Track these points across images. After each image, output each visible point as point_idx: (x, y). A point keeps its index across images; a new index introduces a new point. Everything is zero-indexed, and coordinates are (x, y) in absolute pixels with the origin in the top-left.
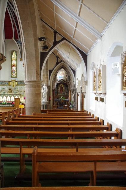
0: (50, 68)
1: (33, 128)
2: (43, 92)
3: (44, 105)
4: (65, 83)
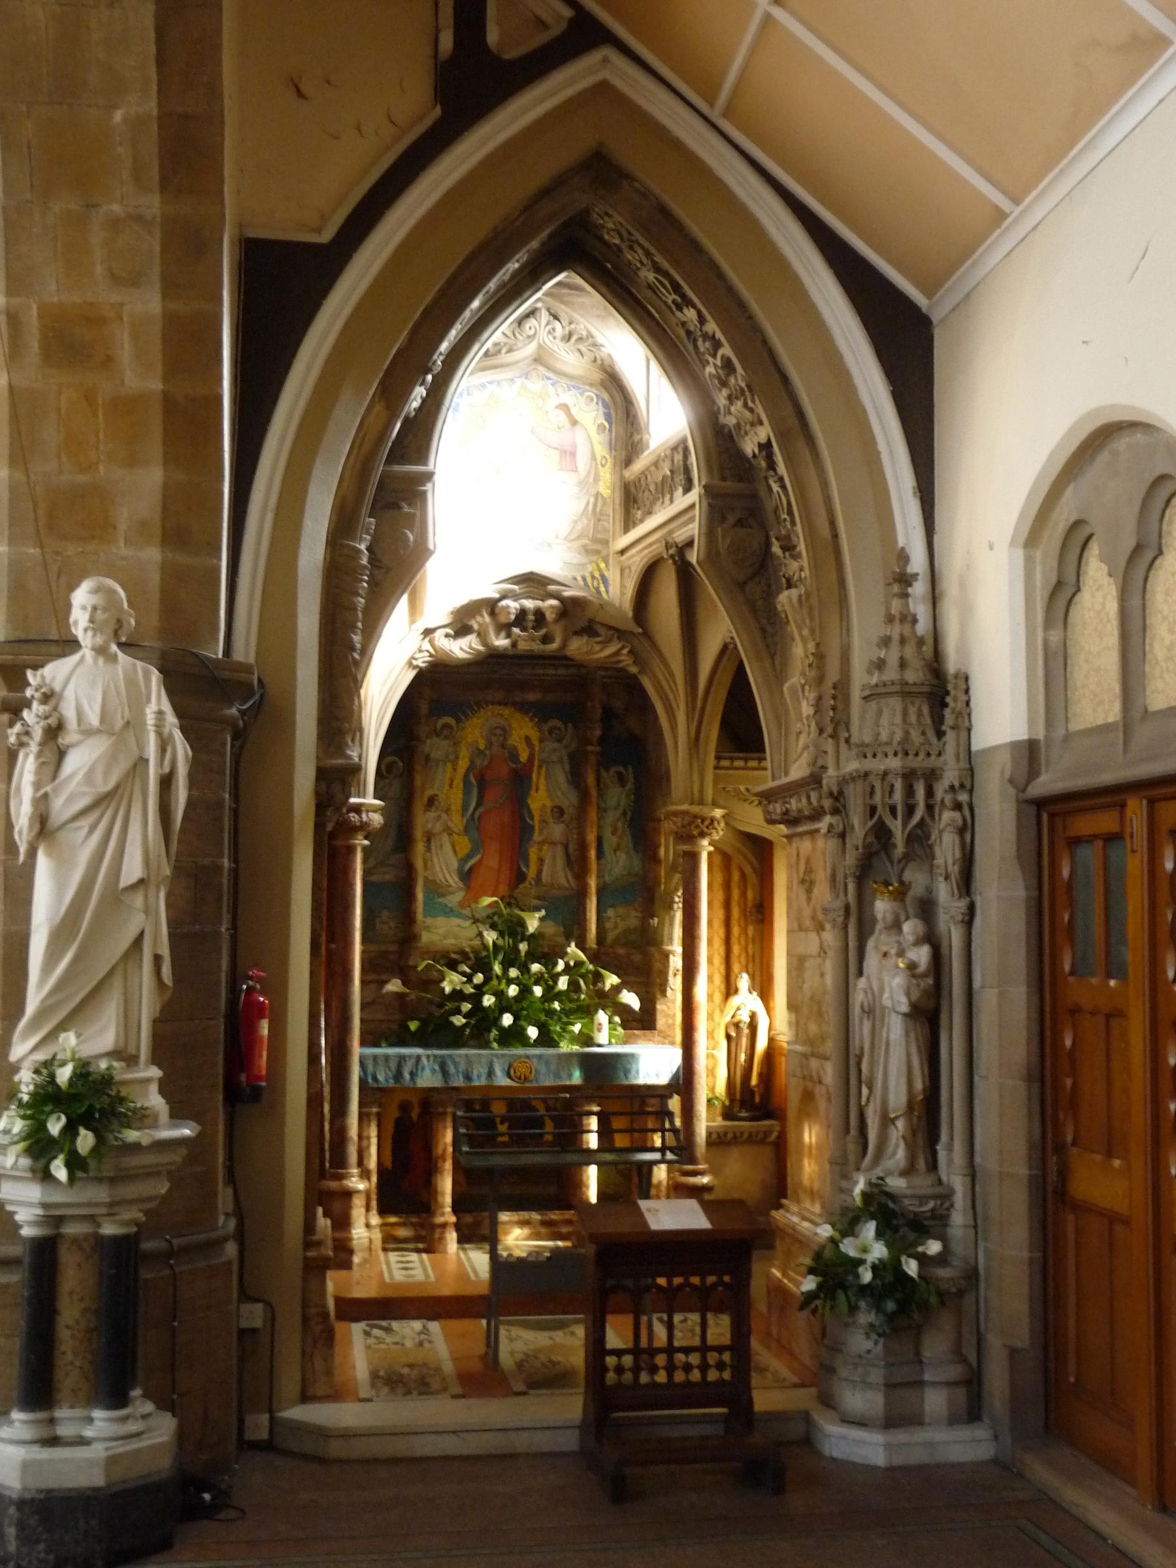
0: (280, 184)
1: (364, 1110)
2: (43, 827)
3: (45, 1252)
4: (603, 652)
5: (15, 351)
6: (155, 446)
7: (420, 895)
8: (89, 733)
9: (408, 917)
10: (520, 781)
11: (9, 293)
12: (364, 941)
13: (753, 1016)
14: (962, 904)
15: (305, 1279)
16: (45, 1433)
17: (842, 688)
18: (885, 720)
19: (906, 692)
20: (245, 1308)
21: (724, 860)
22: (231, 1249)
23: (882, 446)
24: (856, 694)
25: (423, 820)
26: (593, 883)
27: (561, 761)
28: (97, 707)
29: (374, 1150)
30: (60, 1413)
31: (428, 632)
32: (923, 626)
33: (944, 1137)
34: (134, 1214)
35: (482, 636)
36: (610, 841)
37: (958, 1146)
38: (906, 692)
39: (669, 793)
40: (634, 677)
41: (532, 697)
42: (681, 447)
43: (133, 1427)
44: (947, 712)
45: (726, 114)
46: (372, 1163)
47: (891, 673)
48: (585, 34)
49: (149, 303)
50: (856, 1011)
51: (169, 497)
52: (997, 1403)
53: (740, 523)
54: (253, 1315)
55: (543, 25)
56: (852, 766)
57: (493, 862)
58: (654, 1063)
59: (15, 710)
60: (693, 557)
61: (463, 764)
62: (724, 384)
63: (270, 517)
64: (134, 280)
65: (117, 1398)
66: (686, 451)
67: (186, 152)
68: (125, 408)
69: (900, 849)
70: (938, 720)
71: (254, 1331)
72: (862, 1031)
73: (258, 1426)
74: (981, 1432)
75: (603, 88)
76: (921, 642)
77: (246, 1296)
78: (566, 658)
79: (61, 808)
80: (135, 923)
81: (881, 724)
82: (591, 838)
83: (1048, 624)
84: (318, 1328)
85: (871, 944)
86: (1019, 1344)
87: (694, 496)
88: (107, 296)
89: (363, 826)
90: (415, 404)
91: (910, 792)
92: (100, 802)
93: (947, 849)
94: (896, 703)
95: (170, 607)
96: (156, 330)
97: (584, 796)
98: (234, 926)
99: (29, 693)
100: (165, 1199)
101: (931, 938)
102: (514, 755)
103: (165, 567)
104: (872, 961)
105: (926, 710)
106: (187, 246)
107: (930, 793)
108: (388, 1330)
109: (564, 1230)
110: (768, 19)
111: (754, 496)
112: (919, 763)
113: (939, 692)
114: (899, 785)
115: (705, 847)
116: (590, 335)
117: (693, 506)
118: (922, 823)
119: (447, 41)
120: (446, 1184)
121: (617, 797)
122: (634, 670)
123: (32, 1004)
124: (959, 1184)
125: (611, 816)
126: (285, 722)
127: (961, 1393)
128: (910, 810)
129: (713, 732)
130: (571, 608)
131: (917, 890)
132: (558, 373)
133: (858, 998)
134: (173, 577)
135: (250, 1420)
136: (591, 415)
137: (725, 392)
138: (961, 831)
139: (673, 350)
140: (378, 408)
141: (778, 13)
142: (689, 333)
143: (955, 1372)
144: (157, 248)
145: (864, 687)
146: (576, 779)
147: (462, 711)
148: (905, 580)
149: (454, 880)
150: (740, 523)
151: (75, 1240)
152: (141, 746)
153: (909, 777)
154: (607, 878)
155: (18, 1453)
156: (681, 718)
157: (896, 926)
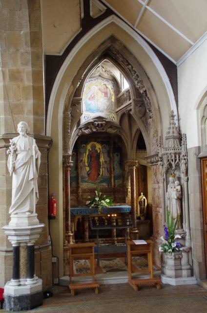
0: (54, 45)
2: (14, 170)
3: (17, 250)
5: (4, 78)
6: (31, 96)
7: (80, 178)
8: (22, 151)
9: (78, 183)
10: (98, 156)
11: (2, 67)
12: (70, 188)
13: (144, 199)
14: (186, 178)
15: (64, 252)
16: (18, 284)
17: (161, 137)
18: (170, 143)
19: (174, 138)
20: (53, 258)
21: (137, 170)
22: (50, 247)
23: (169, 93)
24: (164, 138)
25: (80, 164)
26: (113, 175)
27: (106, 153)
28: (23, 146)
29: (73, 227)
30: (20, 280)
31: (81, 129)
32: (177, 125)
33: (184, 222)
34: (33, 241)
35: (91, 129)
36: (116, 167)
37: (187, 224)
38: (174, 138)
39: (127, 158)
40: (120, 136)
41: (100, 140)
42: (128, 91)
43: (35, 282)
44: (182, 141)
45: (137, 28)
46: (73, 230)
47: (171, 134)
48: (109, 12)
49: (29, 69)
50: (166, 199)
51: (35, 106)
52: (197, 271)
53: (140, 106)
54: (55, 260)
55: (101, 11)
56: (163, 152)
57: (94, 172)
58: (126, 207)
59: (7, 147)
60: (132, 113)
61: (87, 153)
62: (137, 80)
63: (52, 108)
64: (27, 64)
65: (32, 276)
66: (129, 93)
67: (35, 39)
68: (25, 89)
69: (174, 168)
70: (180, 143)
71: (55, 263)
72: (168, 202)
73: (56, 281)
74: (194, 278)
75: (113, 23)
76: (177, 128)
77: (53, 256)
78: (107, 133)
79: (17, 166)
80: (32, 186)
81: (171, 144)
82: (112, 167)
83: (201, 124)
84: (67, 262)
85: (169, 186)
86: (200, 261)
87: (131, 101)
88: (21, 68)
89: (70, 166)
90: (78, 85)
91: (175, 157)
92: (25, 164)
93: (183, 167)
94: (172, 140)
95: (35, 127)
96: (31, 74)
97: (110, 159)
98: (48, 186)
99: (10, 144)
100: (38, 239)
101: (180, 184)
102: (97, 151)
103: (34, 118)
104: (169, 189)
105: (178, 141)
106: (36, 57)
107: (179, 157)
108: (78, 262)
109: (110, 241)
110: (146, 9)
111: (143, 101)
112: (177, 151)
113: (180, 138)
114: (173, 155)
115: (135, 168)
116: (110, 71)
117: (131, 103)
118: (178, 162)
119: (83, 15)
120: (87, 234)
121: (117, 159)
122: (120, 134)
123: (13, 202)
124: (187, 231)
125: (116, 162)
126: (57, 147)
127: (190, 271)
128: (176, 160)
129: (135, 146)
130: (108, 123)
131: (177, 175)
132: (103, 78)
133: (167, 196)
134: (35, 121)
135: (55, 280)
136: (110, 86)
137: (137, 81)
138: (186, 164)
139: (127, 74)
140: (72, 87)
141: (147, 7)
142: (129, 70)
143: (188, 267)
144: (30, 58)
145: (166, 137)
146: (109, 156)
147: (86, 143)
148: (173, 116)
149: (86, 176)
150: (140, 106)
151: (23, 247)
152: (32, 153)
153: (175, 154)
154: (115, 174)
155: (13, 288)
156: (129, 144)
157: (174, 182)
